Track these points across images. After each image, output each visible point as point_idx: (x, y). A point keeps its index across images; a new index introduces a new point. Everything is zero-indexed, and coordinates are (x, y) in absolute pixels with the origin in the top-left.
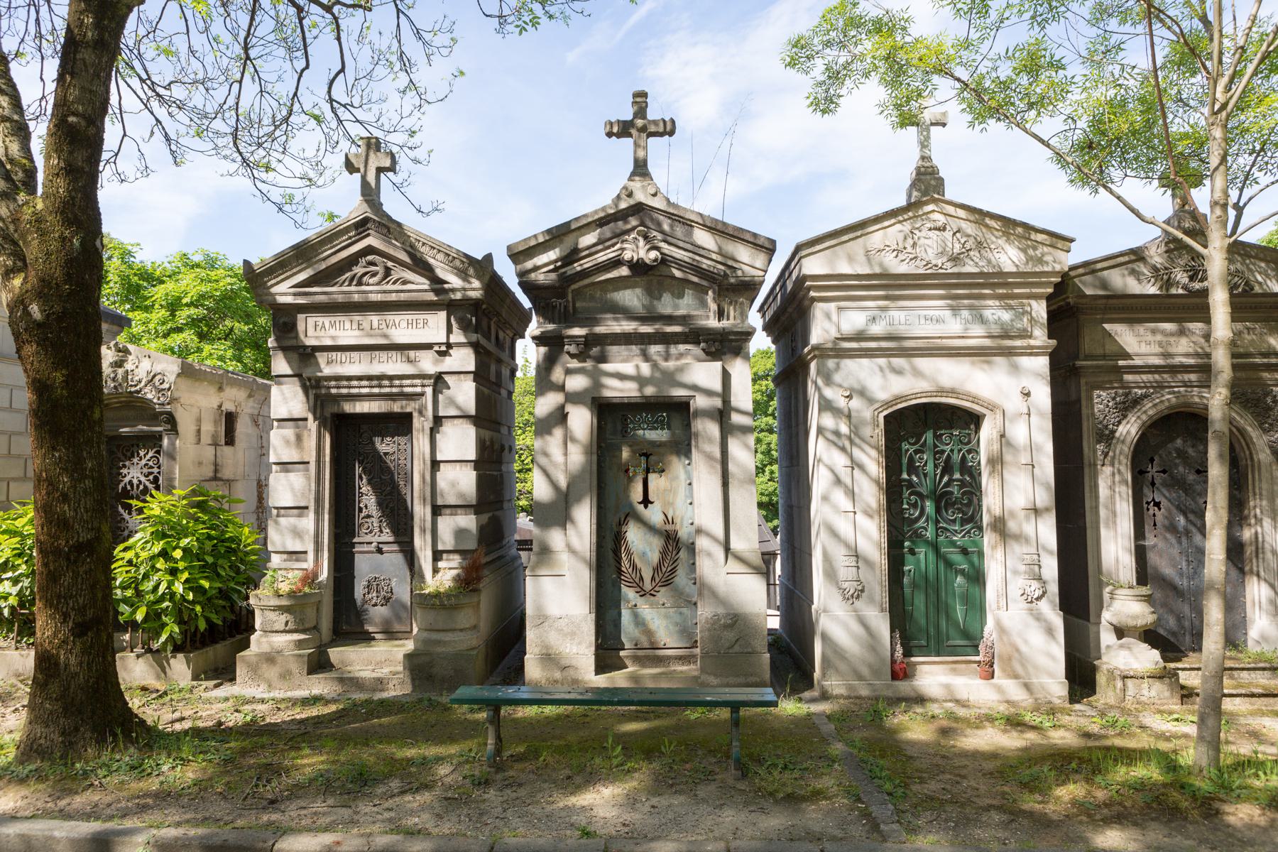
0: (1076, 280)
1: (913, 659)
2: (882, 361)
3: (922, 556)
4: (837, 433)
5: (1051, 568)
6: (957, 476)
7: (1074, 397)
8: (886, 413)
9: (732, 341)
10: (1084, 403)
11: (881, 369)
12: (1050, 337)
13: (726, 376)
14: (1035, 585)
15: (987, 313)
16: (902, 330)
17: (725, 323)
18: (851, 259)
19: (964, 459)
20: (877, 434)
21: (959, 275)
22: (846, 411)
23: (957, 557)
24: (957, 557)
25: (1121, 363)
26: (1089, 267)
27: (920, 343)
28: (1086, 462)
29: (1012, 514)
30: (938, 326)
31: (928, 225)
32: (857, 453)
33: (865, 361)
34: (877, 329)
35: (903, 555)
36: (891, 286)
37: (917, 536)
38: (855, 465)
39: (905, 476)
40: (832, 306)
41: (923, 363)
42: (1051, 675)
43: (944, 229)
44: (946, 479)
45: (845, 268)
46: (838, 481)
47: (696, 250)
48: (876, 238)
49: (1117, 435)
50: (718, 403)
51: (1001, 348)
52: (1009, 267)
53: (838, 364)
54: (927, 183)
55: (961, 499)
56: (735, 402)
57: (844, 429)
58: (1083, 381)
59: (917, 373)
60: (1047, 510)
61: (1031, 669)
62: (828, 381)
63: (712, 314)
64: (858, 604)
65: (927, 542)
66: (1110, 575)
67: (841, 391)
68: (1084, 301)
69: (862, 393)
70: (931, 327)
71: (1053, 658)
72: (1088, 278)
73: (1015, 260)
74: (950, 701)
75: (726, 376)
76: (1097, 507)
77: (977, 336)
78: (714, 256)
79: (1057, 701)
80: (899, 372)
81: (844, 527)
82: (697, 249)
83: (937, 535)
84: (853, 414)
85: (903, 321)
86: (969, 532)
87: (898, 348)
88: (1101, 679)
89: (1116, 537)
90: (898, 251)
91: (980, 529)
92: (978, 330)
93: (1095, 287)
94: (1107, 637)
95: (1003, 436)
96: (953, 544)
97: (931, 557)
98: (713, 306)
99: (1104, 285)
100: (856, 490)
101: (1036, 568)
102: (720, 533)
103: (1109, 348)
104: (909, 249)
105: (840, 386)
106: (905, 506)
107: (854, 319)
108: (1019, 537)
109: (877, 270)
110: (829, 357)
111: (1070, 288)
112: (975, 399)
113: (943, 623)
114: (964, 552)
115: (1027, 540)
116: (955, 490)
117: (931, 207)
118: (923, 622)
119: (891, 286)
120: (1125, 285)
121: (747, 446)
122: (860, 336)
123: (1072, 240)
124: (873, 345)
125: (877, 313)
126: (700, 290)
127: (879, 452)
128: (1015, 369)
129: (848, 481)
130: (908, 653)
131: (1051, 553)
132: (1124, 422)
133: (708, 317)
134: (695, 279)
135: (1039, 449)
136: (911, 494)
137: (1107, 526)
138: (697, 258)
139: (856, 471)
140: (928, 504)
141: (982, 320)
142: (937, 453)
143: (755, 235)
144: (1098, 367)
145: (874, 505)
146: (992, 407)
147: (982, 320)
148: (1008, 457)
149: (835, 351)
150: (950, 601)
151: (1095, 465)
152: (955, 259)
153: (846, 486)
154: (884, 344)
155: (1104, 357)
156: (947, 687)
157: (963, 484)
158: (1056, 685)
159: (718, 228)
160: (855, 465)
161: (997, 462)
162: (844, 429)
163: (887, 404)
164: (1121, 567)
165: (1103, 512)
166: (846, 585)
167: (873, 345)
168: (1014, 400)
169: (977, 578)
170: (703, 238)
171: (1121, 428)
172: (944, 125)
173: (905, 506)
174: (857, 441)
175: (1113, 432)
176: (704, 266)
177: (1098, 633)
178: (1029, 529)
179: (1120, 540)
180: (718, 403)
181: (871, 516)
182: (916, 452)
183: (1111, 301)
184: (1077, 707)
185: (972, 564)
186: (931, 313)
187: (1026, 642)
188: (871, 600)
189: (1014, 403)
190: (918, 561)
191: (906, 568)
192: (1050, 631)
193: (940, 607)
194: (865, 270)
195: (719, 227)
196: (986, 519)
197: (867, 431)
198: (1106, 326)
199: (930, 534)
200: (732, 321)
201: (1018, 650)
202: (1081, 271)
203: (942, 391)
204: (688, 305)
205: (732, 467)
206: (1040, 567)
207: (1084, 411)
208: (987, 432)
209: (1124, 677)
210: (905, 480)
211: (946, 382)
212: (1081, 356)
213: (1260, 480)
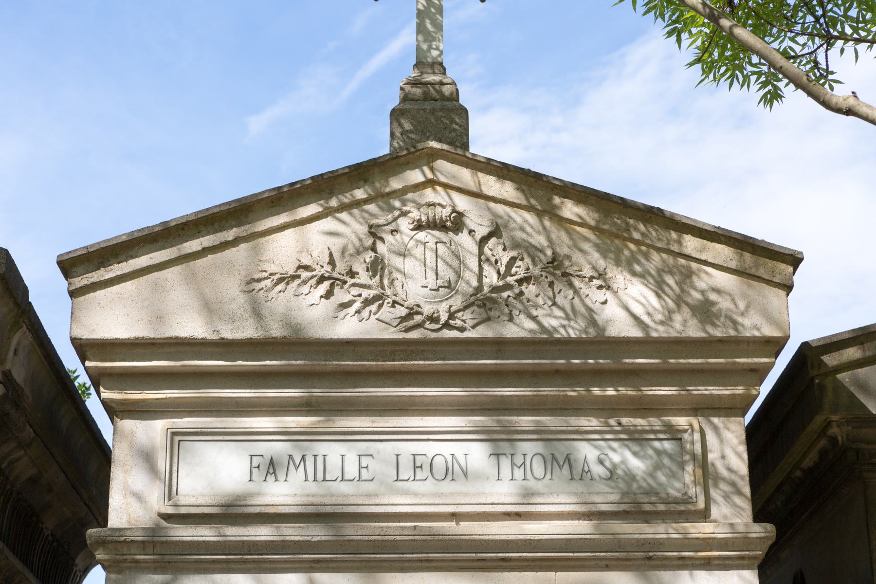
12: (758, 517)
15: (587, 452)
16: (347, 493)
21: (500, 346)
30: (447, 487)
31: (415, 214)
34: (281, 493)
36: (323, 377)
45: (191, 326)
52: (620, 326)
54: (431, 118)
73: (638, 310)
104: (363, 277)
107: (216, 470)
119: (323, 377)
122: (232, 512)
124: (262, 533)
125: (278, 448)
141: (579, 475)
152: (485, 303)
154: (292, 532)
167: (262, 533)
186: (429, 449)
202: (852, 353)
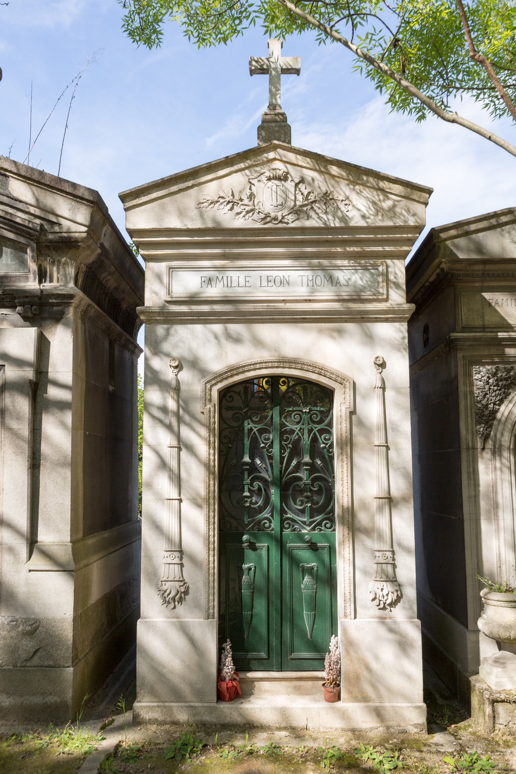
0: (448, 243)
1: (251, 675)
2: (218, 328)
3: (264, 552)
4: (164, 409)
5: (408, 568)
6: (307, 459)
7: (453, 374)
8: (220, 386)
9: (53, 305)
10: (461, 379)
11: (216, 337)
12: (409, 301)
13: (43, 346)
14: (388, 588)
15: (341, 276)
16: (240, 292)
17: (47, 285)
18: (182, 213)
19: (315, 441)
20: (208, 410)
21: (303, 230)
22: (174, 383)
23: (305, 555)
24: (305, 555)
25: (501, 335)
26: (462, 228)
27: (259, 307)
28: (463, 445)
29: (365, 507)
30: (281, 289)
31: (268, 174)
32: (186, 432)
33: (198, 328)
34: (213, 292)
35: (243, 550)
36: (227, 243)
37: (259, 528)
38: (182, 445)
39: (247, 459)
40: (162, 267)
41: (267, 331)
42: (406, 698)
43: (285, 179)
44: (294, 462)
45: (174, 222)
46: (163, 465)
47: (12, 203)
48: (212, 188)
49: (499, 415)
50: (29, 374)
51: (351, 314)
52: (357, 221)
53: (168, 330)
55: (312, 489)
56: (52, 374)
57: (172, 404)
58: (460, 355)
59: (258, 342)
60: (404, 500)
61: (383, 691)
62: (155, 347)
63: (31, 276)
64: (181, 609)
65: (271, 536)
66: (492, 577)
67: (167, 360)
68: (458, 266)
69: (195, 364)
70: (274, 289)
71: (409, 678)
72: (462, 241)
74: (285, 728)
75: (43, 346)
76: (476, 497)
77: (325, 298)
78: (32, 210)
79: (413, 730)
80: (237, 340)
81: (167, 519)
82: (14, 202)
83: (282, 528)
84: (183, 387)
85: (242, 282)
86: (319, 524)
87: (237, 312)
88: (475, 701)
89: (498, 531)
90: (233, 203)
91: (332, 521)
92: (326, 293)
93: (469, 250)
94: (487, 650)
95: (353, 413)
96: (300, 538)
97: (275, 553)
98: (33, 266)
99: (479, 248)
100: (183, 475)
101: (390, 568)
102: (23, 522)
103: (489, 320)
104: (246, 201)
105: (168, 355)
106: (247, 494)
107: (188, 281)
108: (368, 532)
109: (210, 225)
110: (158, 322)
111: (442, 251)
112: (321, 371)
113: (287, 631)
114: (313, 547)
115: (381, 537)
116: (303, 475)
117: (271, 155)
118: (263, 630)
119: (227, 243)
120: (503, 249)
121: (63, 424)
122: (192, 300)
123: (430, 192)
124: (205, 308)
125: (213, 274)
126: (19, 249)
127: (210, 430)
128: (369, 338)
129: (174, 464)
130: (242, 665)
131: (407, 550)
132: (506, 402)
133: (27, 278)
134: (11, 236)
135: (395, 429)
136: (252, 481)
137: (489, 519)
138: (11, 211)
139: (184, 453)
140: (272, 491)
141: (332, 280)
142: (284, 432)
143: (74, 185)
144: (475, 339)
145: (202, 491)
146: (341, 380)
147: (332, 280)
148: (359, 439)
149: (168, 317)
150: (296, 606)
151: (474, 448)
152: (298, 212)
153: (171, 470)
154: (218, 308)
155: (483, 328)
156: (283, 712)
157: (313, 468)
158: (411, 713)
159: (35, 179)
160: (182, 445)
161: (349, 443)
162: (172, 404)
163: (220, 376)
164: (504, 568)
165: (483, 504)
166: (167, 586)
167: (205, 308)
168: (370, 371)
169: (328, 579)
170: (19, 189)
171: (502, 408)
172: (297, 72)
173: (247, 494)
174: (187, 418)
175: (495, 412)
176: (18, 220)
177: (477, 642)
178: (382, 522)
179: (502, 534)
180: (29, 374)
181: (200, 506)
182: (261, 431)
183: (489, 267)
184: (438, 738)
185: (321, 561)
186: (274, 274)
187: (377, 657)
188: (197, 605)
189: (367, 378)
190: (260, 557)
191: (245, 566)
192: (403, 645)
193: (283, 611)
194: (197, 225)
195: (35, 176)
196: (337, 511)
197: (197, 408)
198: (487, 296)
199: (275, 525)
200: (55, 284)
201: (368, 669)
202: (453, 232)
203: (284, 362)
204: (7, 265)
205: (45, 448)
206: (394, 566)
207: (462, 389)
208: (340, 407)
209: (494, 702)
210: (246, 464)
211: (290, 351)
212: (458, 328)
213: (289, 293)
